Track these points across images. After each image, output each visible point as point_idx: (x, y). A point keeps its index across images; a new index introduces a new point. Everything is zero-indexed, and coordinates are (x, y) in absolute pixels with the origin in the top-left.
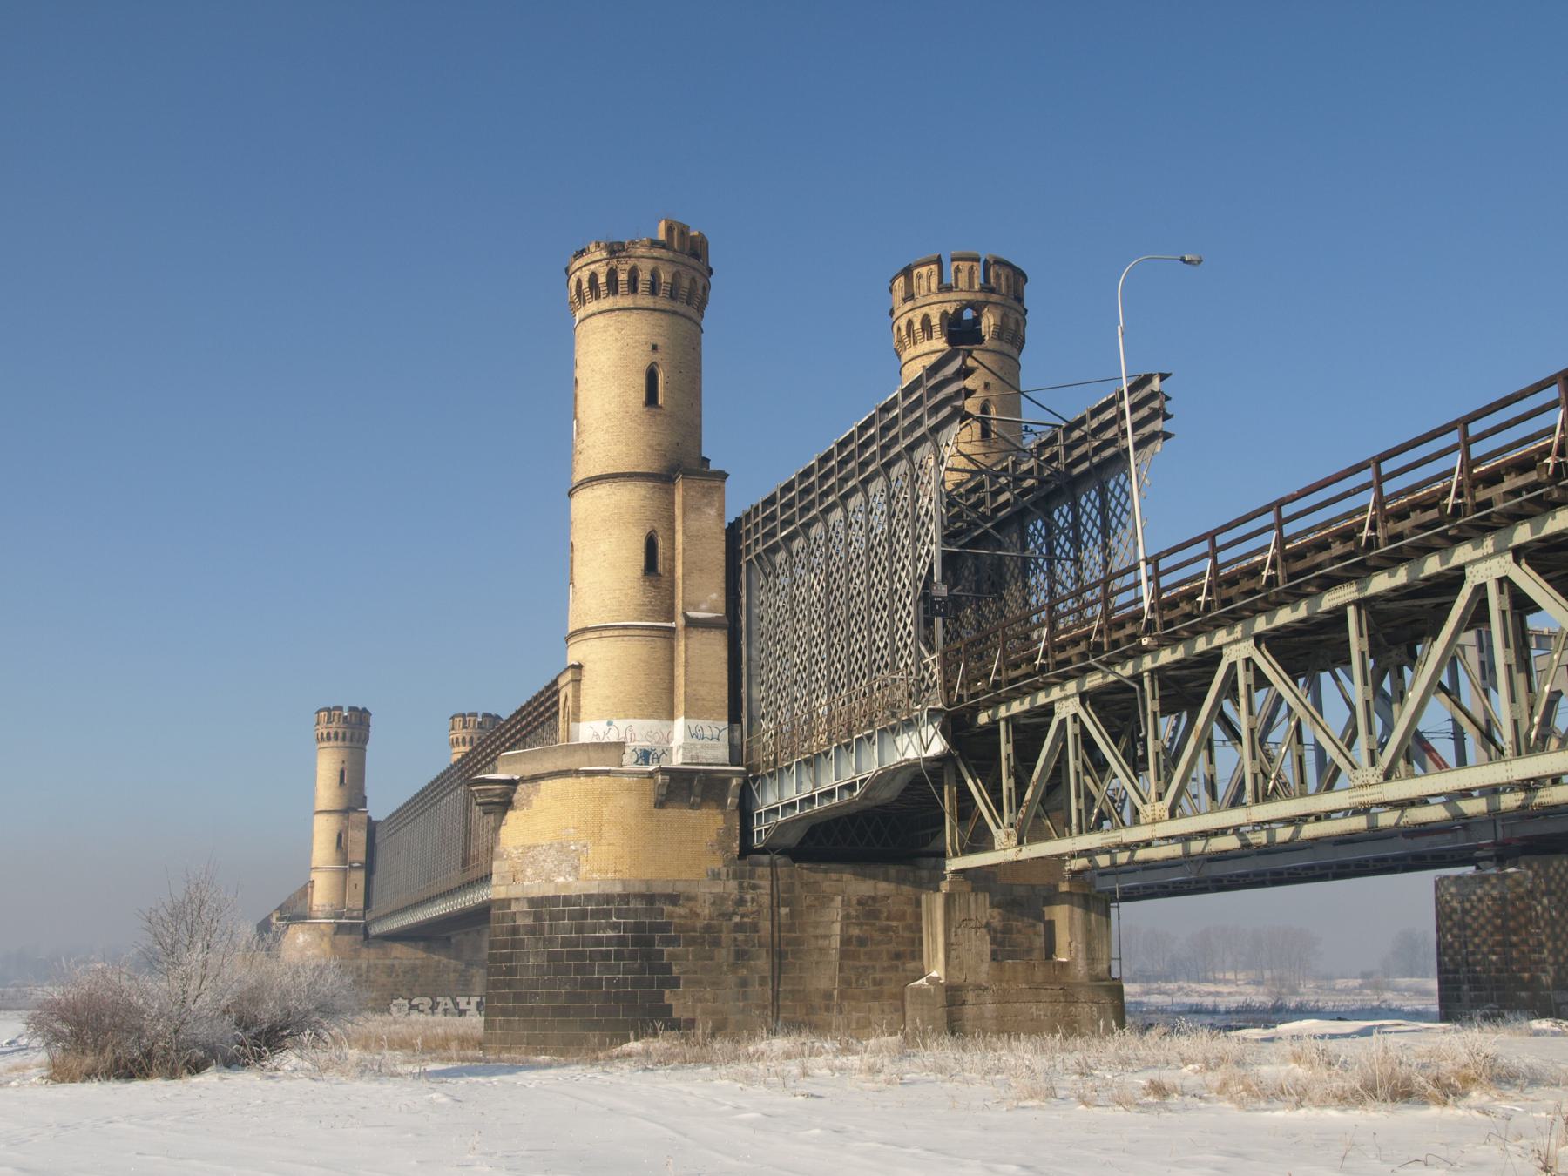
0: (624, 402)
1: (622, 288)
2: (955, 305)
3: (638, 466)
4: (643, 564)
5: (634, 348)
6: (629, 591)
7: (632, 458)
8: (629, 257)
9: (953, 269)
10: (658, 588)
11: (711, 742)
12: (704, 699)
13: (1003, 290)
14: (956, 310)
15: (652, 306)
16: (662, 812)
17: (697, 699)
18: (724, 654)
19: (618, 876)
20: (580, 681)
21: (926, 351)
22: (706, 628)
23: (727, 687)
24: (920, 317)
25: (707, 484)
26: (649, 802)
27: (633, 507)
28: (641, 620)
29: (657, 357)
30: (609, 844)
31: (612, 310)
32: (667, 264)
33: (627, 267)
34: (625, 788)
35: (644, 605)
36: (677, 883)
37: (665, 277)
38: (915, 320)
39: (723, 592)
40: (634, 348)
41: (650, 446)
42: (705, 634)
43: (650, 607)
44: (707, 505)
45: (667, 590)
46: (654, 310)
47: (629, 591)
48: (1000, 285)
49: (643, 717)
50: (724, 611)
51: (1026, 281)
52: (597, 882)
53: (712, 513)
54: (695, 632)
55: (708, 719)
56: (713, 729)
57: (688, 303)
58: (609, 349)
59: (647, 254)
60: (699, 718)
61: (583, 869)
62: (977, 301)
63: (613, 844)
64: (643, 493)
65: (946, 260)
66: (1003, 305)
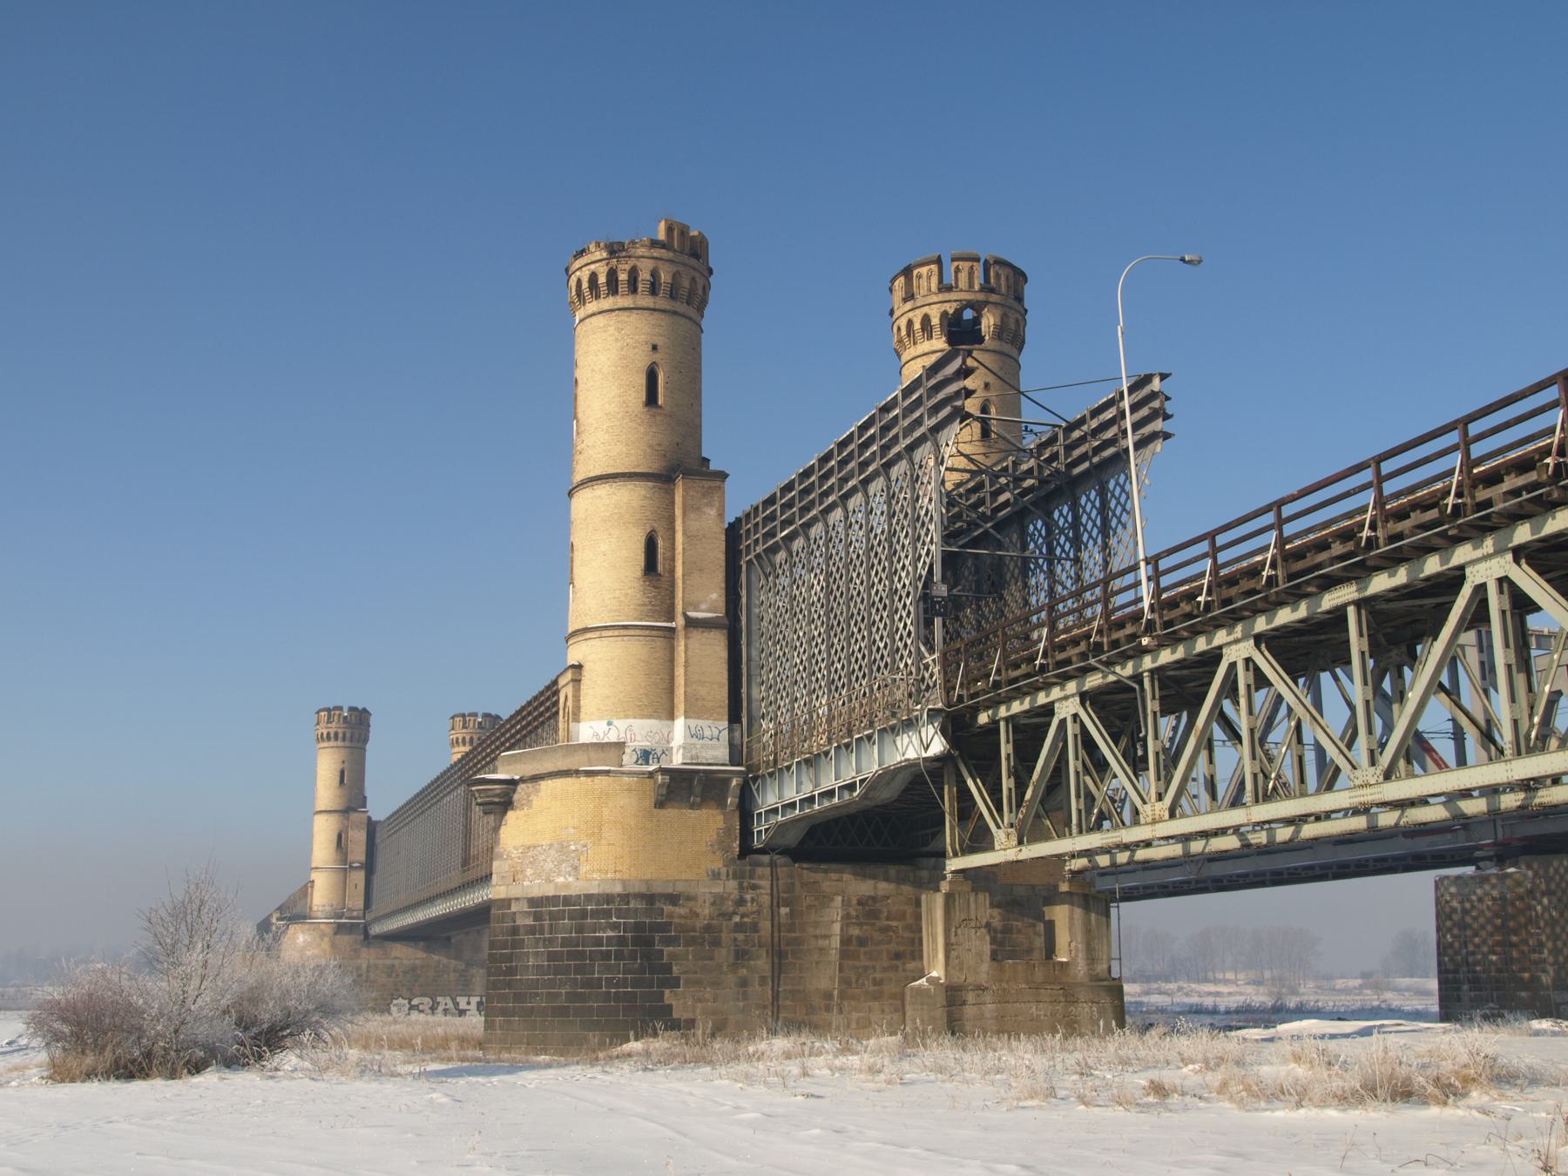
0: (624, 402)
1: (622, 288)
2: (955, 305)
3: (638, 466)
4: (643, 564)
5: (634, 348)
6: (629, 591)
7: (632, 458)
8: (629, 257)
9: (953, 269)
10: (658, 588)
11: (711, 742)
12: (704, 699)
13: (1003, 290)
14: (956, 310)
15: (652, 306)
16: (662, 812)
17: (697, 699)
18: (724, 654)
19: (618, 876)
20: (580, 681)
21: (926, 351)
22: (706, 628)
23: (727, 687)
24: (920, 317)
25: (707, 484)
26: (649, 802)
27: (633, 507)
28: (641, 620)
29: (657, 357)
30: (609, 844)
31: (612, 310)
32: (667, 264)
33: (627, 267)
34: (625, 788)
35: (644, 605)
36: (677, 883)
37: (665, 277)
38: (915, 320)
39: (723, 592)
40: (634, 348)
41: (650, 446)
42: (705, 634)
43: (650, 607)
44: (707, 505)
45: (667, 590)
46: (654, 310)
47: (629, 591)
48: (1000, 285)
49: (643, 717)
50: (724, 611)
51: (1026, 281)
52: (597, 882)
53: (712, 513)
54: (695, 632)
55: (708, 719)
56: (713, 729)
57: (688, 303)
58: (609, 349)
59: (647, 254)
60: (699, 718)
61: (583, 869)
62: (977, 301)
63: (613, 844)
64: (643, 493)
65: (946, 260)
66: (1003, 305)
